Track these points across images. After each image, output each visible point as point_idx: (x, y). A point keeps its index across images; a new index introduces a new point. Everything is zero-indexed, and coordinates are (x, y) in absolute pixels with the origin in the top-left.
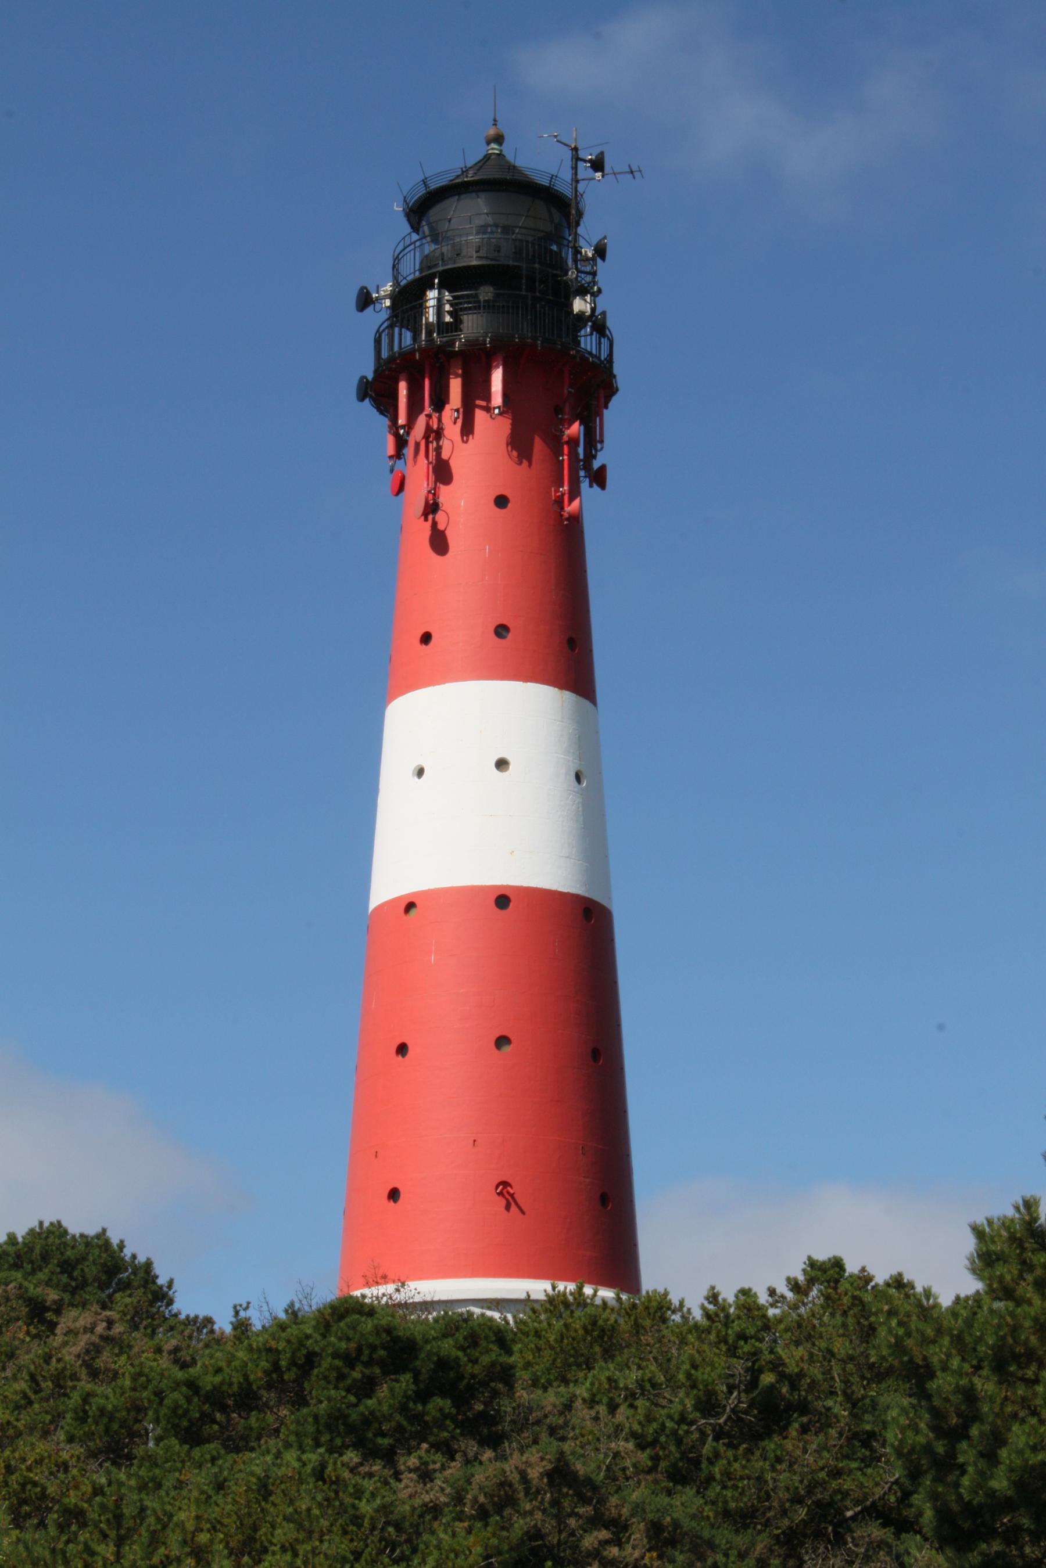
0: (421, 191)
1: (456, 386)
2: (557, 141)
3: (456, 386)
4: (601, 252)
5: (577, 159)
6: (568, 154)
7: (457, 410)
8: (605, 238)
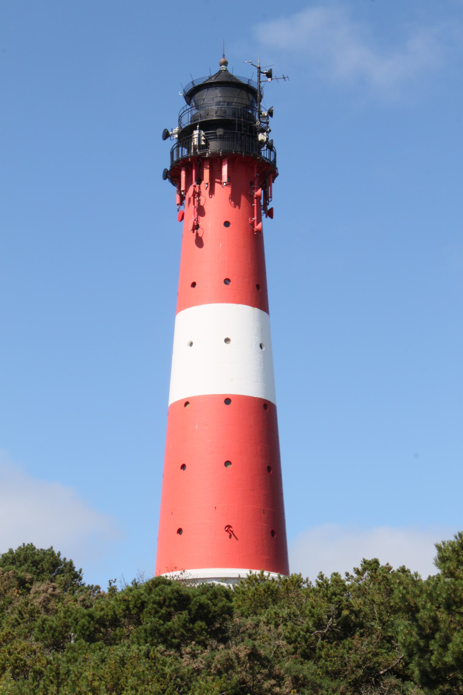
0: (191, 87)
1: (206, 173)
2: (251, 64)
3: (206, 173)
4: (271, 113)
5: (260, 72)
6: (256, 70)
7: (207, 184)
8: (272, 107)
